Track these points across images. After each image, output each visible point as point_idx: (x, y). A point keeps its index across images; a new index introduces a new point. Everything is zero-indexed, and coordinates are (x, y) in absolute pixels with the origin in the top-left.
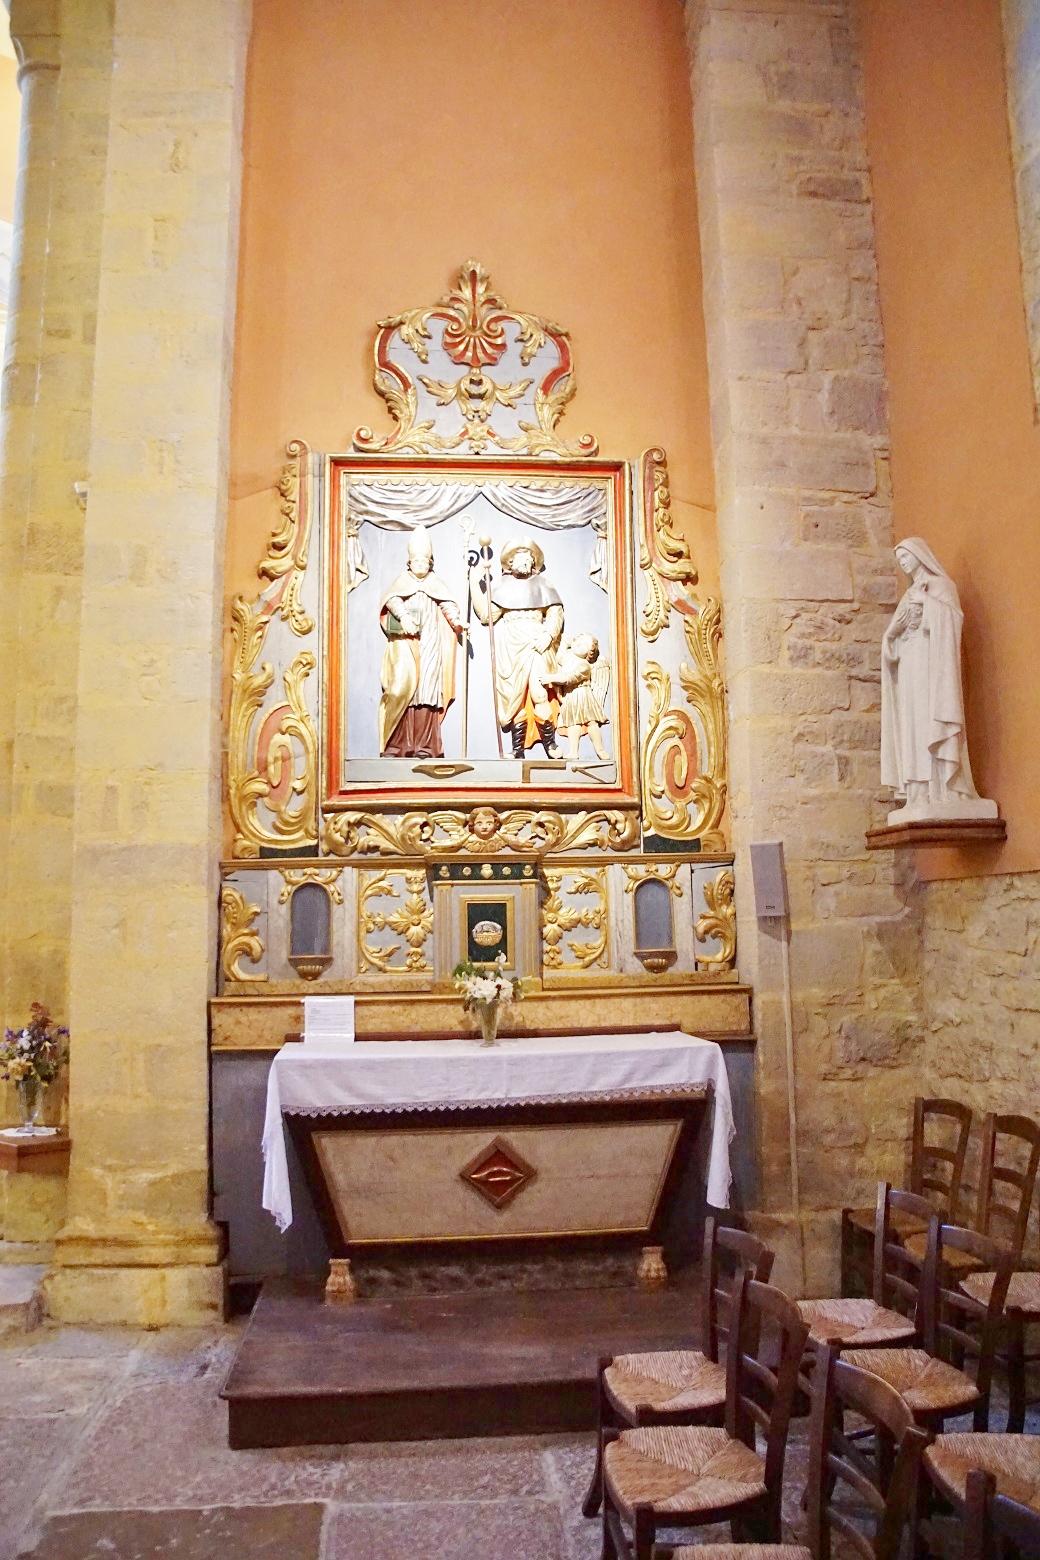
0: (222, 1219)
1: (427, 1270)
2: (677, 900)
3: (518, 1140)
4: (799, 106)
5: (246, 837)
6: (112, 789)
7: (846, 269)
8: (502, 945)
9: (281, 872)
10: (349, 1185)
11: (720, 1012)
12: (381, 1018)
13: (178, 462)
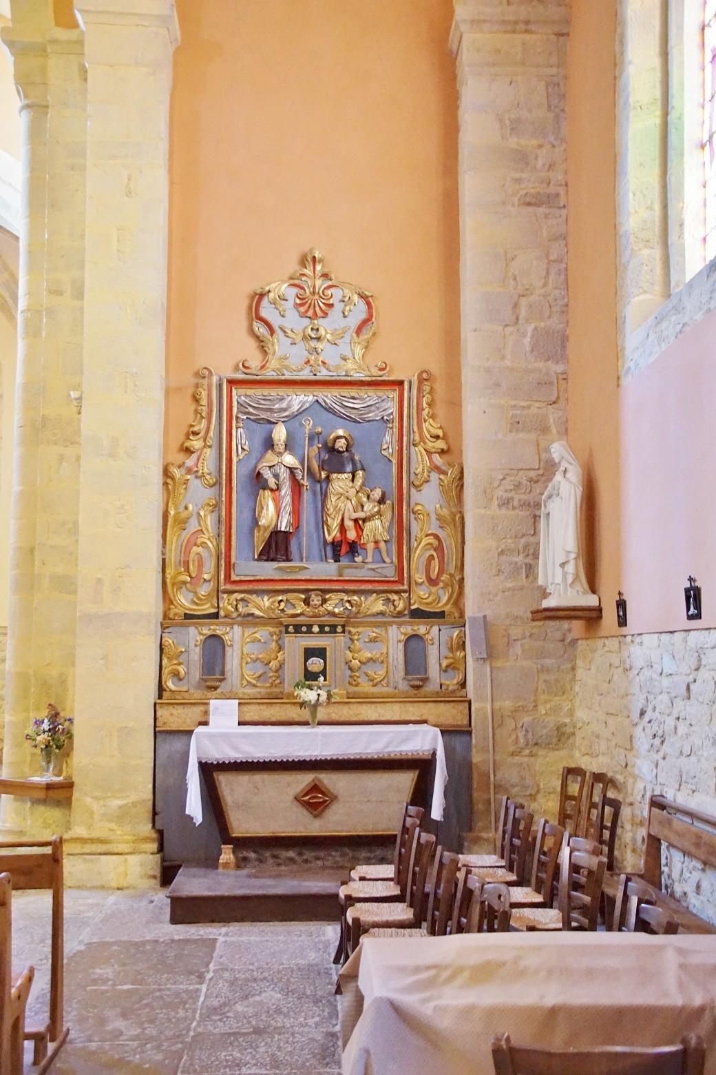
0: (160, 828)
1: (275, 853)
2: (430, 647)
3: (329, 780)
4: (523, 142)
5: (176, 607)
6: (99, 581)
7: (547, 256)
8: (324, 673)
9: (197, 628)
10: (233, 802)
11: (451, 714)
12: (253, 713)
13: (135, 385)
